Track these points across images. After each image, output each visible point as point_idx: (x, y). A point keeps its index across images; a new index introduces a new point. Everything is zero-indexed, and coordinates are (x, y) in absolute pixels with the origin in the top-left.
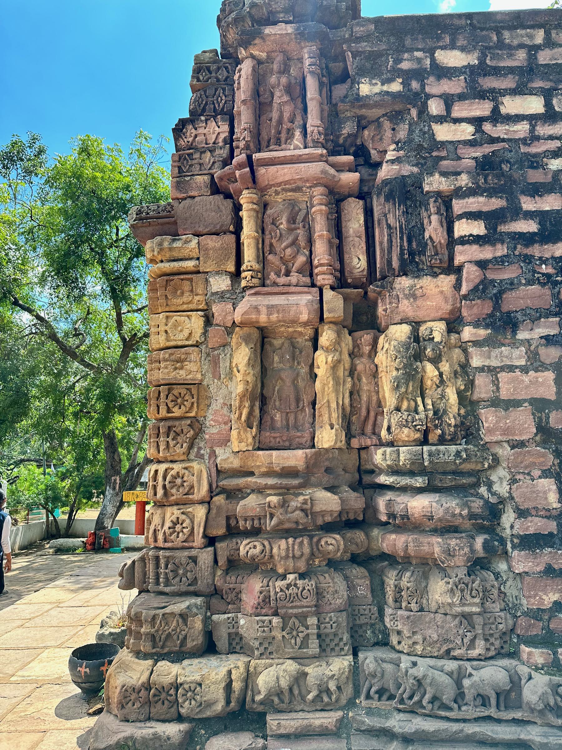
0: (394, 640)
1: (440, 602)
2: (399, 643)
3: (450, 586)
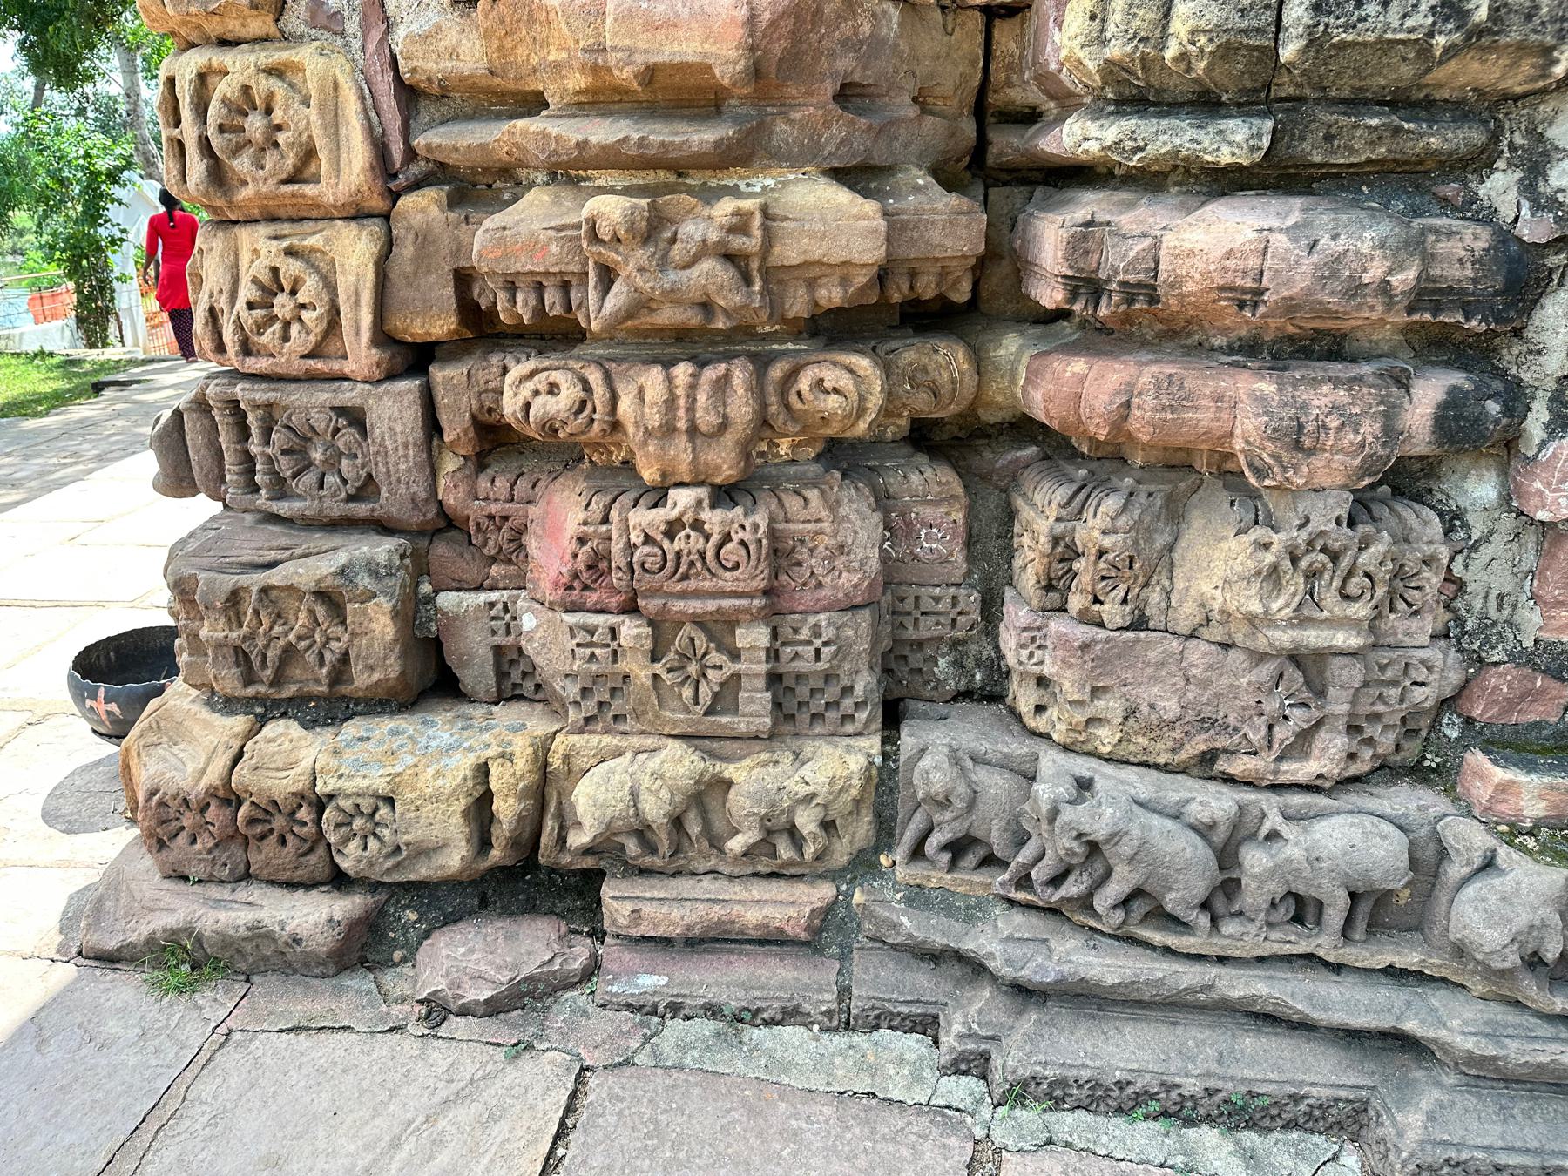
0: (1024, 698)
1: (1216, 606)
2: (1040, 709)
3: (1269, 558)
